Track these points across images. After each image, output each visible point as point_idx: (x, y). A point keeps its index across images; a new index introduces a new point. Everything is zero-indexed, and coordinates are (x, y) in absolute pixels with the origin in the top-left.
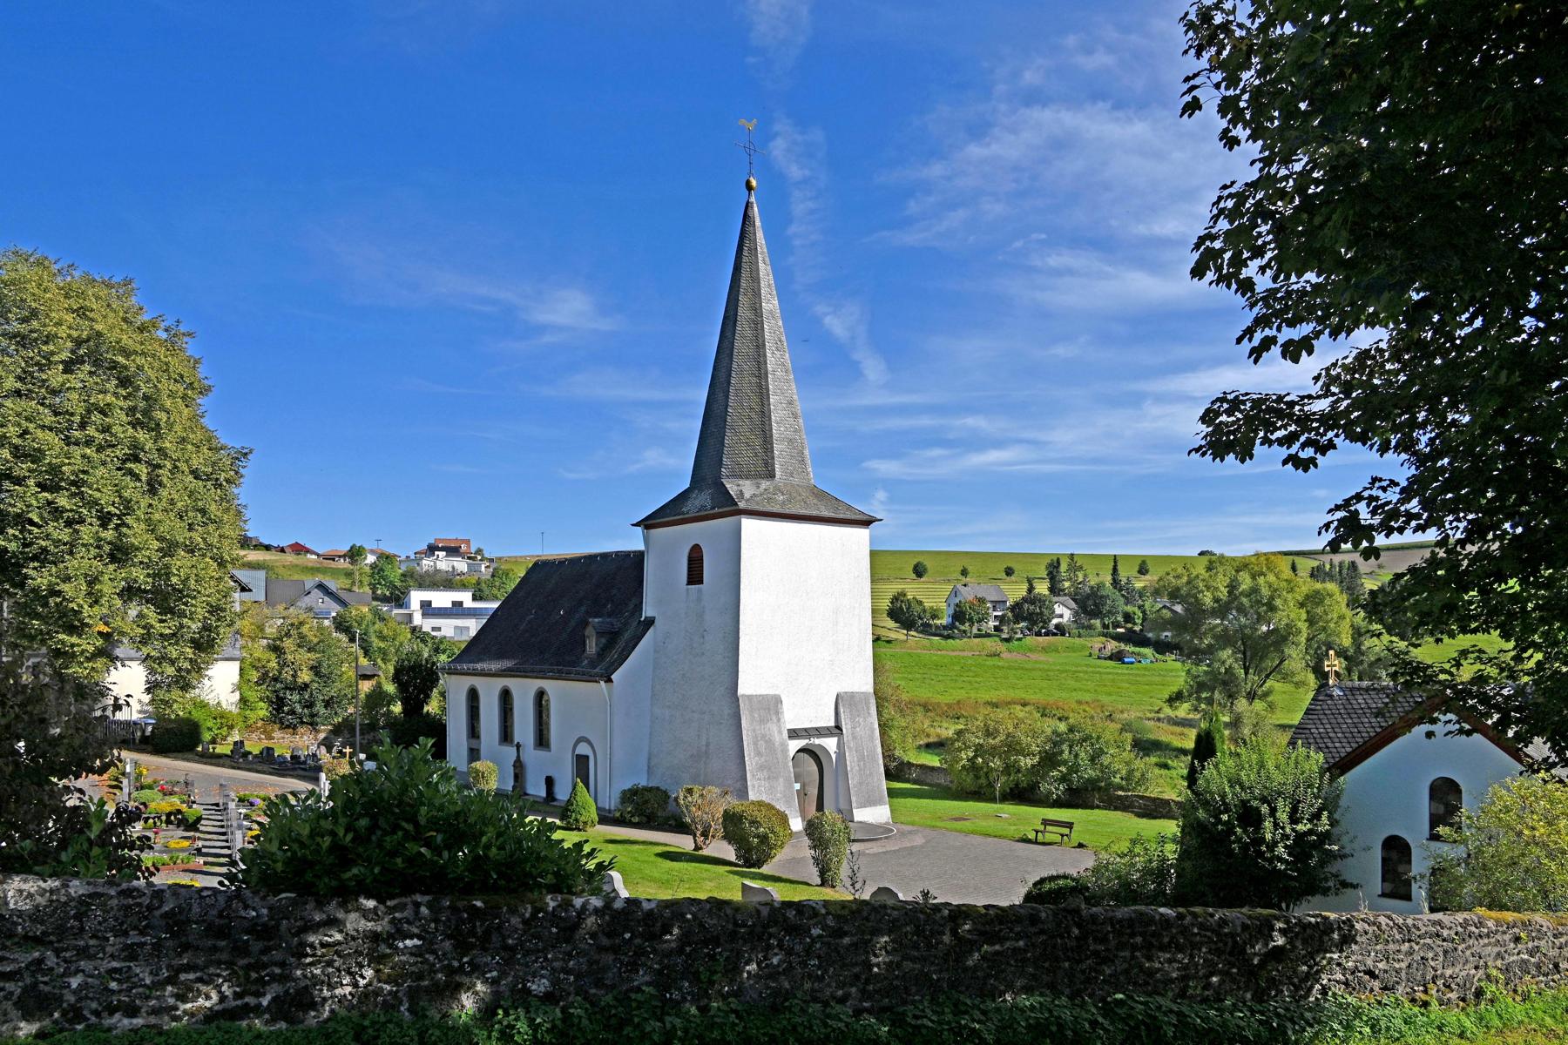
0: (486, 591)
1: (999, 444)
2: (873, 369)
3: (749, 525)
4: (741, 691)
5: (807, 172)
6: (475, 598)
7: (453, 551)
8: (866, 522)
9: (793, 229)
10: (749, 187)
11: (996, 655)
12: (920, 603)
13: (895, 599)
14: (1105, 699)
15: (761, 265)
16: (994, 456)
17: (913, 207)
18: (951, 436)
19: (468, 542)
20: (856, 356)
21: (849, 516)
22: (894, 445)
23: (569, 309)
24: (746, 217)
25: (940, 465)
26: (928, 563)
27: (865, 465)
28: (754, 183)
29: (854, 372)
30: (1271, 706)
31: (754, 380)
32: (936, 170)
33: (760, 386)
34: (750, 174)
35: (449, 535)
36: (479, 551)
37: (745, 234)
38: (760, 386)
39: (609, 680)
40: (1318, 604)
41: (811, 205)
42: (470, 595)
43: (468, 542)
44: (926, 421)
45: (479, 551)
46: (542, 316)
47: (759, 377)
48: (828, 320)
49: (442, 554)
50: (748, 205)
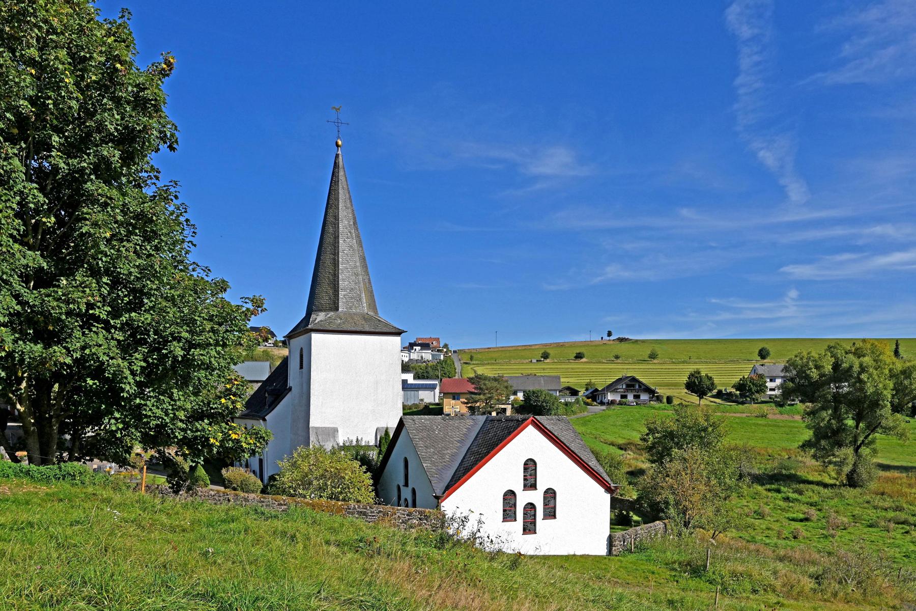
0: (431, 373)
1: (903, 247)
2: (796, 191)
3: (315, 337)
4: (311, 425)
5: (756, 31)
6: (414, 378)
7: (425, 346)
8: (398, 333)
9: (739, 80)
10: (338, 146)
11: (763, 416)
12: (710, 378)
13: (691, 376)
14: (594, 432)
15: (341, 191)
16: (897, 257)
17: (847, 49)
18: (860, 242)
19: (438, 340)
20: (782, 182)
21: (385, 330)
22: (810, 252)
23: (556, 162)
24: (336, 165)
25: (850, 267)
26: (551, 352)
27: (782, 270)
28: (340, 143)
29: (781, 194)
30: (875, 451)
31: (332, 256)
32: (873, 14)
33: (334, 259)
34: (339, 137)
35: (424, 335)
36: (446, 346)
37: (334, 174)
38: (334, 259)
39: (264, 420)
40: (906, 378)
41: (756, 58)
42: (412, 375)
43: (438, 340)
44: (839, 231)
45: (446, 346)
46: (537, 169)
47: (334, 255)
48: (762, 154)
49: (418, 348)
50: (337, 156)
